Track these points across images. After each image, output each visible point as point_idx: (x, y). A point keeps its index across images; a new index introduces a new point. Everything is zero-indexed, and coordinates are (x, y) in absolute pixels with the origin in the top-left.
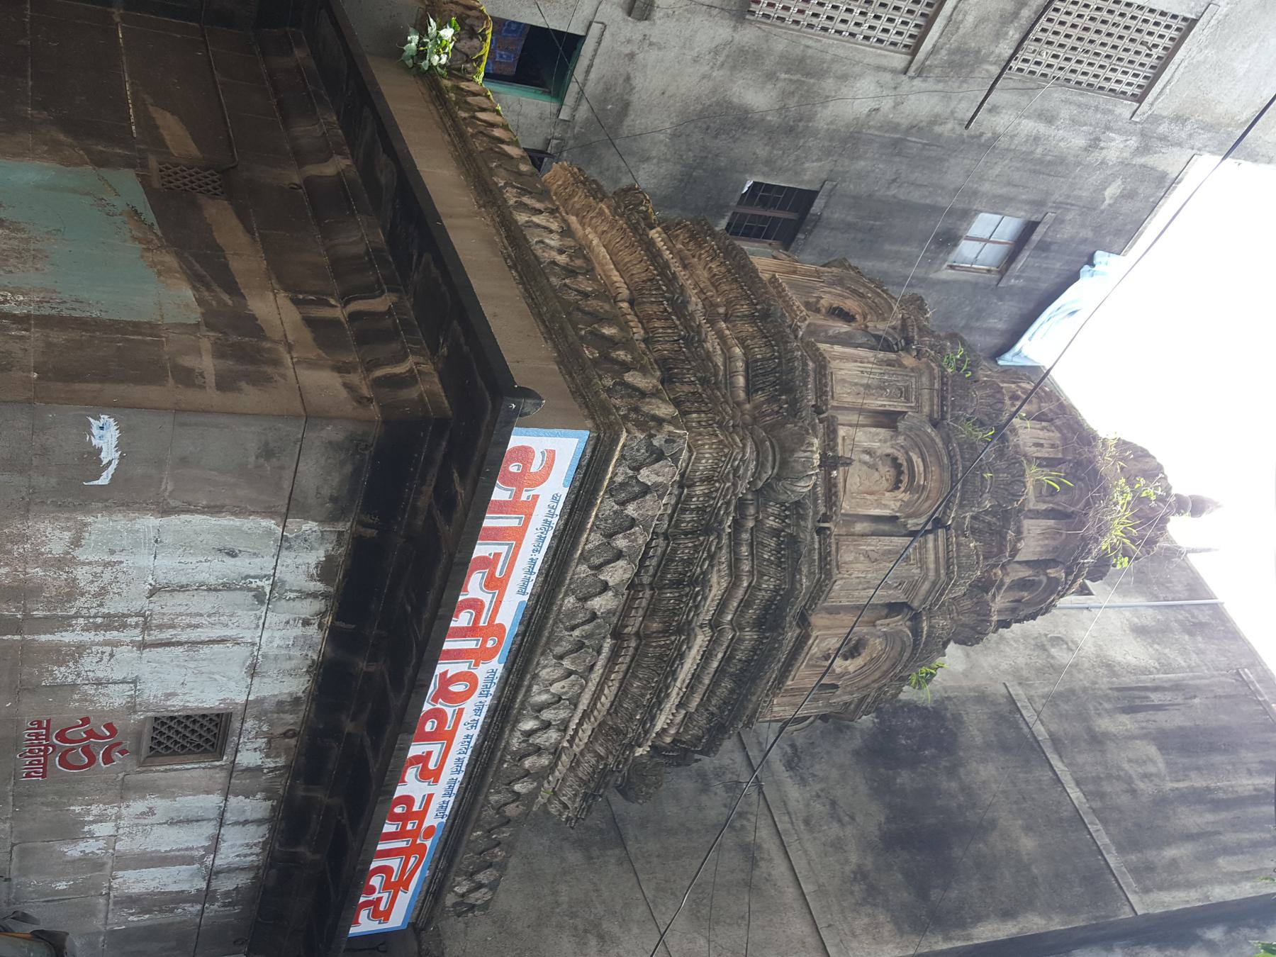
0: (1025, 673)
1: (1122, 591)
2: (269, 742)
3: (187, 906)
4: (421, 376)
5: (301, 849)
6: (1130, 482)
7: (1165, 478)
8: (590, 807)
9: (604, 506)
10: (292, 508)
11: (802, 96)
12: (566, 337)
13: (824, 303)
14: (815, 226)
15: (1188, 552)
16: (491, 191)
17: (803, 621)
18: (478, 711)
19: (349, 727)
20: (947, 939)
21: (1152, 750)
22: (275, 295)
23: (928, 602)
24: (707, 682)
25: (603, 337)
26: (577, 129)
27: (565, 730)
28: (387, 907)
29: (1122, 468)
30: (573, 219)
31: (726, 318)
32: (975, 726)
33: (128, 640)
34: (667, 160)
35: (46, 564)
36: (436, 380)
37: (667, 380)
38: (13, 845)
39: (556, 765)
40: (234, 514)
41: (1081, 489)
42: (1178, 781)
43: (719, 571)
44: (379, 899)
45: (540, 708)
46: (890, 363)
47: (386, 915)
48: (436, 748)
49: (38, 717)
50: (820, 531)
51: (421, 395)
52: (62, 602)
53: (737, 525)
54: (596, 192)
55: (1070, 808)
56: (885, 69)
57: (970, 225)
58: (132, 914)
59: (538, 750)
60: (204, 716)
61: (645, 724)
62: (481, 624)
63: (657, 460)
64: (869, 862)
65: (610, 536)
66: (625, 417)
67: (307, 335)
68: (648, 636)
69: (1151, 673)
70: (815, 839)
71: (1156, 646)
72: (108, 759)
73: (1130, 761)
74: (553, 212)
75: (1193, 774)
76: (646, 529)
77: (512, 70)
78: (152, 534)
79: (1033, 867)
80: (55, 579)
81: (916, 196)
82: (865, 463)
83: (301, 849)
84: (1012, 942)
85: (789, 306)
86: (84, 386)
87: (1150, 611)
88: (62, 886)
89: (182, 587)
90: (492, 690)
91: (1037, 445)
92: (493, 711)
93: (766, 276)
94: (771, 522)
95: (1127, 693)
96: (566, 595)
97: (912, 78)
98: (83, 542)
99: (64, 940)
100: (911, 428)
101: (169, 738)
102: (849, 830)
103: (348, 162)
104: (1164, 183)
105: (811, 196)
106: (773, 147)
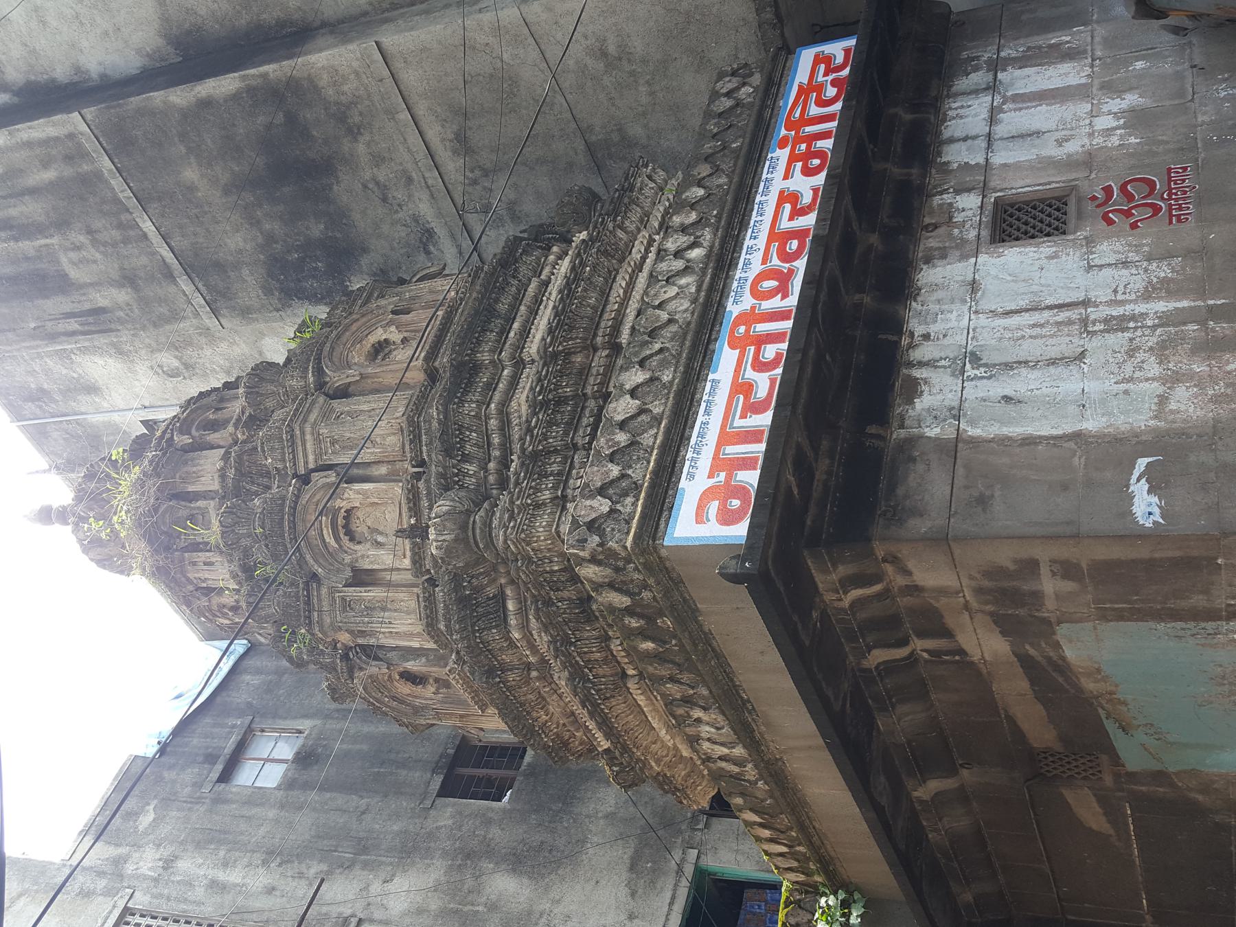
0: (203, 340)
1: (114, 429)
2: (951, 218)
3: (1014, 54)
4: (835, 587)
5: (908, 117)
6: (115, 534)
7: (80, 541)
8: (626, 179)
9: (642, 472)
10: (953, 449)
11: (460, 890)
12: (691, 637)
13: (431, 689)
14: (437, 763)
15: (50, 470)
16: (771, 775)
17: (432, 376)
18: (747, 263)
19: (874, 239)
20: (264, 76)
21: (73, 273)
22: (983, 658)
23: (309, 401)
24: (522, 308)
25: (653, 640)
26: (679, 841)
27: (659, 251)
28: (819, 69)
29: (123, 547)
30: (686, 753)
31: (529, 667)
32: (249, 285)
33: (1101, 307)
34: (588, 816)
35: (1191, 376)
36: (820, 585)
37: (585, 601)
38: (1192, 100)
39: (663, 217)
40: (1009, 438)
41: (164, 523)
42: (46, 245)
43: (520, 417)
44: (826, 74)
45: (686, 270)
46: (363, 633)
47: (818, 60)
48: (785, 224)
49: (1183, 225)
50: (422, 464)
51: (834, 565)
52: (1170, 340)
53: (505, 463)
54: (664, 783)
55: (151, 211)
56: (380, 922)
57: (285, 775)
58: (1068, 42)
59: (684, 229)
60: (1017, 239)
61: (580, 263)
62: (753, 348)
63: (593, 521)
64: (346, 145)
65: (633, 444)
66: (628, 560)
67: (950, 621)
68: (585, 348)
69: (79, 349)
70: (401, 164)
71: (75, 375)
72: (1108, 191)
73: (95, 262)
74: (708, 759)
75: (32, 253)
76: (598, 452)
77: (748, 893)
78: (1089, 412)
79: (184, 150)
80: (1180, 361)
81: (340, 799)
82: (381, 533)
83: (908, 117)
84: (200, 77)
85: (467, 684)
86: (1170, 554)
87: (83, 409)
88: (1139, 65)
89: (1053, 363)
90: (735, 284)
91: (211, 564)
92: (733, 264)
93: (491, 710)
94: (471, 468)
95: (101, 327)
96: (671, 382)
97: (353, 916)
98: (1156, 400)
99: (1137, 11)
100: (338, 570)
101: (1049, 215)
102: (367, 175)
103: (916, 794)
104: (100, 829)
105: (444, 792)
106: (485, 837)
